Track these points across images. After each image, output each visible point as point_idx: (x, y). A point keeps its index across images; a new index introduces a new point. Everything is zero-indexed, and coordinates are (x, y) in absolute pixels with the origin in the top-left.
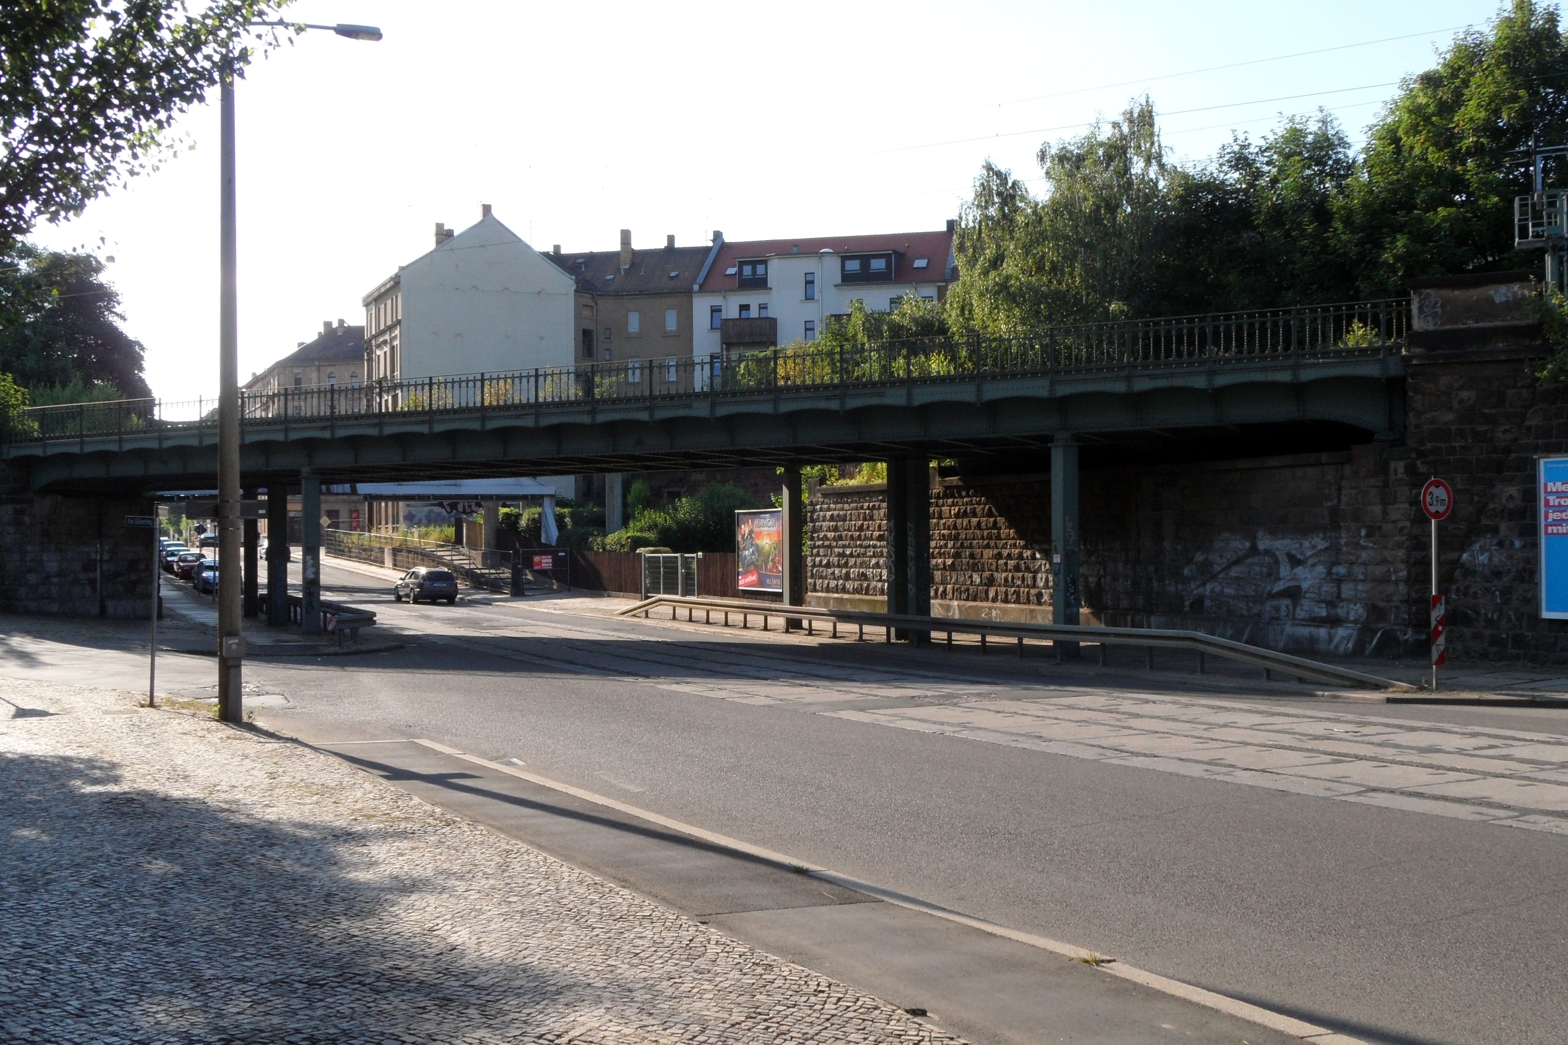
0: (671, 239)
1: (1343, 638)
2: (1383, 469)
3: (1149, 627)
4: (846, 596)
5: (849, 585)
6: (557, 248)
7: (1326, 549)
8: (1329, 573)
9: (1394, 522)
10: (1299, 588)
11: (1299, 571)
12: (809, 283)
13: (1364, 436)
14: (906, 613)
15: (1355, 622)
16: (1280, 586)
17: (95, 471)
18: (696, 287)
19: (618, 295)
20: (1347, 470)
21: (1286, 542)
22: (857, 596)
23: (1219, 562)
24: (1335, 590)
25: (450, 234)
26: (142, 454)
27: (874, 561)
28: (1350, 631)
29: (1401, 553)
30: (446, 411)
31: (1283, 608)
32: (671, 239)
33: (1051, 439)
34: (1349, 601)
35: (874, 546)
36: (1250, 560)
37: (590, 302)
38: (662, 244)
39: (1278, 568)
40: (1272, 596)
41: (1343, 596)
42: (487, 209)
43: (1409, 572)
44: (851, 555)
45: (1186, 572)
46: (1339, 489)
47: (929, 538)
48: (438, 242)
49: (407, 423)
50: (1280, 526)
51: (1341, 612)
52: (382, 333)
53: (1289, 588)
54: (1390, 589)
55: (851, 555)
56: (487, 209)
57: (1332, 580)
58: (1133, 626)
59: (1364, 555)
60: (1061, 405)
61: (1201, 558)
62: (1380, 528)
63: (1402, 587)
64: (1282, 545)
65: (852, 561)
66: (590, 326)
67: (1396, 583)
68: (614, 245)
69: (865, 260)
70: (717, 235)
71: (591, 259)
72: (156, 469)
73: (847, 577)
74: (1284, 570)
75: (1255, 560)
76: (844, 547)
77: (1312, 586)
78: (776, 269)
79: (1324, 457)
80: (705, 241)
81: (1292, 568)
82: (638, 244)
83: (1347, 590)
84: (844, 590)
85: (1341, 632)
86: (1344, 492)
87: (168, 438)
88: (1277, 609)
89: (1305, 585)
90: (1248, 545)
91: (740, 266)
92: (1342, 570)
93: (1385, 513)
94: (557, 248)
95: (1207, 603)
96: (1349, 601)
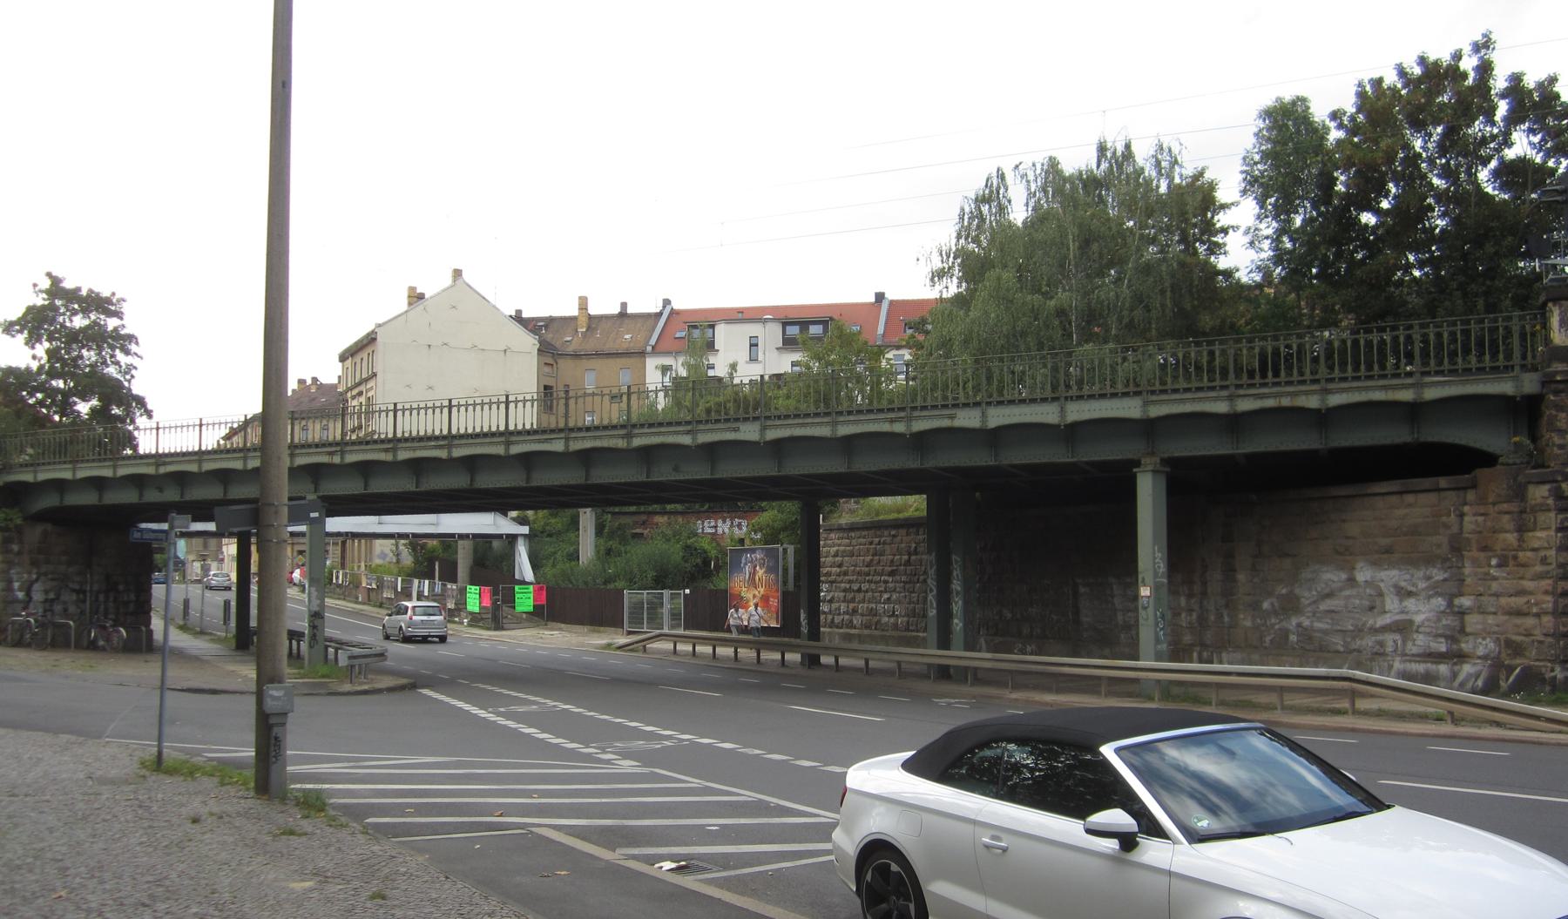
0: (624, 305)
1: (1469, 676)
2: (1519, 493)
3: (1221, 662)
4: (853, 631)
5: (857, 620)
6: (519, 312)
7: (1445, 580)
8: (1450, 604)
9: (1534, 550)
10: (1411, 622)
11: (1410, 604)
12: (754, 345)
13: (1489, 460)
14: (948, 648)
15: (1485, 658)
16: (1387, 620)
17: (88, 498)
18: (649, 349)
19: (576, 356)
20: (1471, 495)
21: (1395, 572)
22: (866, 632)
23: (1306, 595)
24: (1457, 623)
25: (421, 297)
26: (138, 481)
27: (886, 596)
28: (1479, 668)
29: (1546, 584)
30: (466, 436)
31: (1390, 643)
32: (624, 305)
33: (1137, 464)
34: (1475, 635)
35: (886, 582)
36: (1347, 593)
37: (550, 361)
38: (616, 310)
39: (1383, 602)
40: (1375, 631)
41: (1468, 630)
42: (457, 273)
43: (1556, 603)
44: (859, 590)
45: (1266, 605)
46: (1462, 516)
47: (819, 591)
48: (410, 304)
49: (424, 448)
50: (1384, 556)
51: (1466, 646)
52: (359, 384)
53: (1396, 622)
54: (1530, 622)
55: (859, 590)
56: (457, 273)
57: (1454, 613)
58: (1201, 661)
59: (1495, 586)
60: (1148, 428)
61: (1284, 591)
62: (1515, 558)
63: (1548, 621)
64: (1390, 576)
65: (860, 596)
66: (550, 382)
67: (1538, 615)
68: (572, 310)
69: (804, 324)
70: (667, 302)
71: (550, 322)
72: (152, 496)
73: (855, 611)
74: (1392, 603)
75: (1354, 592)
76: (850, 582)
77: (1428, 620)
78: (722, 333)
79: (1443, 482)
80: (653, 307)
81: (1401, 601)
82: (593, 310)
83: (1473, 622)
84: (851, 625)
85: (1467, 669)
86: (1466, 519)
87: (165, 464)
88: (1381, 644)
89: (1418, 619)
90: (1344, 576)
91: (694, 331)
92: (1466, 602)
93: (1521, 540)
94: (519, 312)
95: (1293, 638)
96: (1475, 635)
